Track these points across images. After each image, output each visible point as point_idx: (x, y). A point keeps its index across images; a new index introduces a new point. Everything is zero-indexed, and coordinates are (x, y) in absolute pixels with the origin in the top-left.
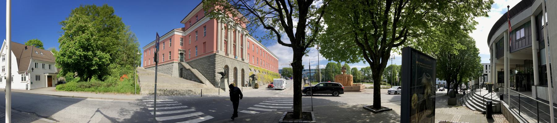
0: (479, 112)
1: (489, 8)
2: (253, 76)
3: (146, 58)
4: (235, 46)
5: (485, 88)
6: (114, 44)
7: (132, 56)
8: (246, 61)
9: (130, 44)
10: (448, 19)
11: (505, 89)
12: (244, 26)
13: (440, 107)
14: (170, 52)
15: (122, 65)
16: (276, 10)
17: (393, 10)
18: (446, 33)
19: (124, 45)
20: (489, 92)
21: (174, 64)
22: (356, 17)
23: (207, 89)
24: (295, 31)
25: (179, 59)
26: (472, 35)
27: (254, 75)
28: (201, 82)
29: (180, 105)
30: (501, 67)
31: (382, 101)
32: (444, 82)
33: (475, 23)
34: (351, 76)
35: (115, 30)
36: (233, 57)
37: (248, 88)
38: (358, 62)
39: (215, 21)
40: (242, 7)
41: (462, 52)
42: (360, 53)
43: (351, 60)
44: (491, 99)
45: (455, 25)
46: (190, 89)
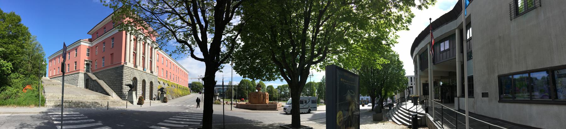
0: (405, 127)
1: (409, 21)
2: (162, 90)
3: (52, 69)
4: (144, 59)
5: (411, 101)
6: (18, 53)
7: (38, 65)
8: (155, 73)
9: (36, 54)
10: (369, 35)
11: (429, 102)
12: (154, 39)
13: (365, 123)
14: (76, 62)
15: (26, 75)
16: (188, 24)
17: (311, 28)
18: (368, 48)
19: (29, 55)
20: (414, 105)
21: (80, 75)
22: (274, 35)
23: (114, 102)
24: (209, 46)
25: (85, 69)
26: (395, 49)
27: (163, 88)
28: (108, 94)
29: (86, 119)
30: (426, 79)
31: (301, 120)
32: (367, 98)
33: (396, 37)
34: (267, 93)
35: (20, 38)
36: (142, 69)
37: (157, 101)
38: (274, 80)
39: (124, 32)
40: (153, 21)
41: (384, 66)
42: (276, 72)
43: (266, 77)
44: (416, 112)
45: (377, 41)
46: (96, 101)
